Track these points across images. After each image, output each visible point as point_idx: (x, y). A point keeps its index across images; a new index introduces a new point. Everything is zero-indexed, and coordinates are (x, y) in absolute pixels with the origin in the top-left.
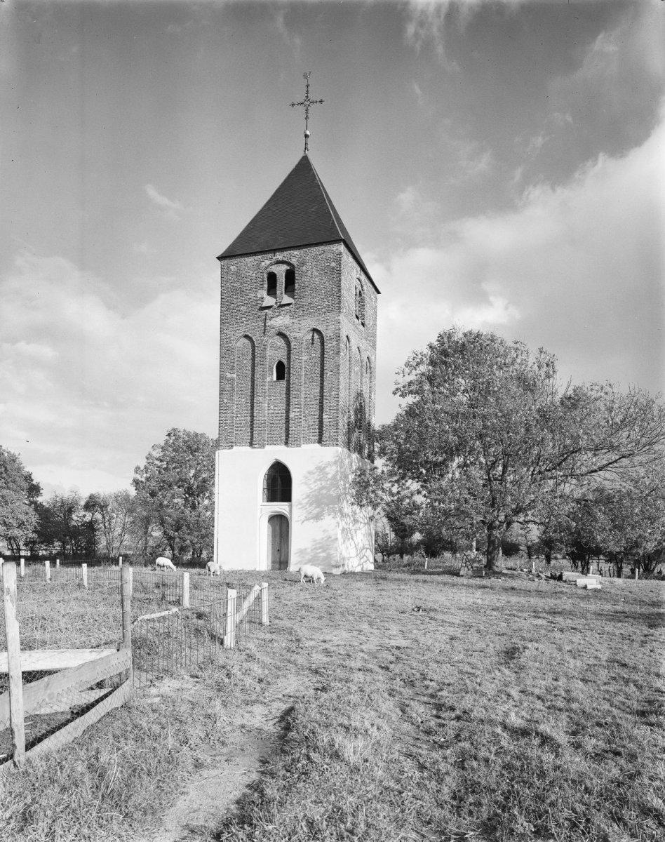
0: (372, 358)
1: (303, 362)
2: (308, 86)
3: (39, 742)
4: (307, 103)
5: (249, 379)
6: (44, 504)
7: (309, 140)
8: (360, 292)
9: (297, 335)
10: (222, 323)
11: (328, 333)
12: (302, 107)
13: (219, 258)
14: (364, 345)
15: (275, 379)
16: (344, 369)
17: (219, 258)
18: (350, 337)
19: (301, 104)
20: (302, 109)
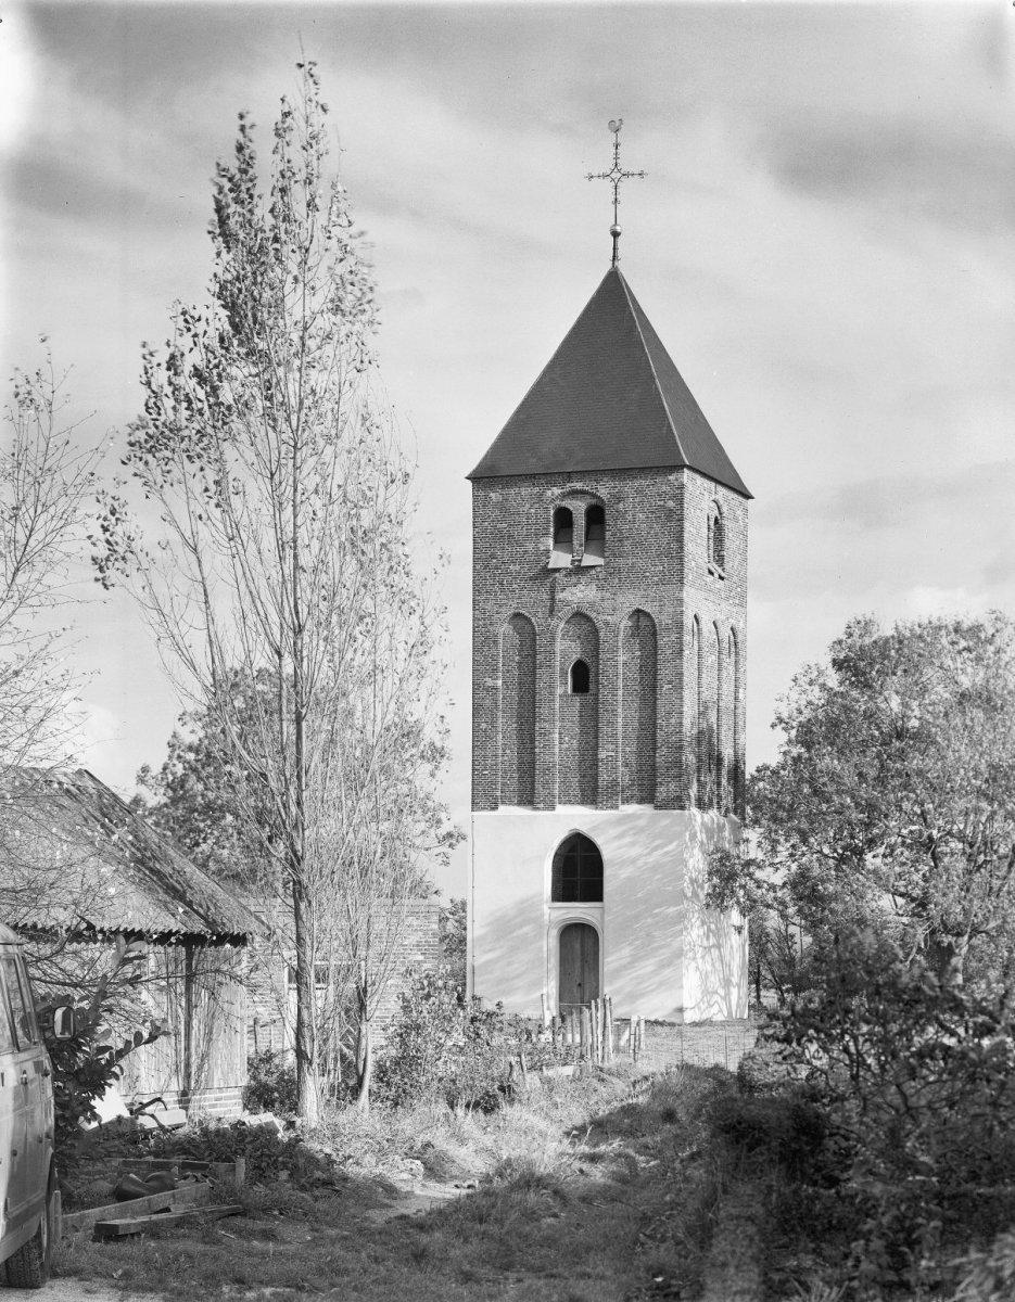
1: (620, 662)
18: (700, 616)
20: (608, 185)
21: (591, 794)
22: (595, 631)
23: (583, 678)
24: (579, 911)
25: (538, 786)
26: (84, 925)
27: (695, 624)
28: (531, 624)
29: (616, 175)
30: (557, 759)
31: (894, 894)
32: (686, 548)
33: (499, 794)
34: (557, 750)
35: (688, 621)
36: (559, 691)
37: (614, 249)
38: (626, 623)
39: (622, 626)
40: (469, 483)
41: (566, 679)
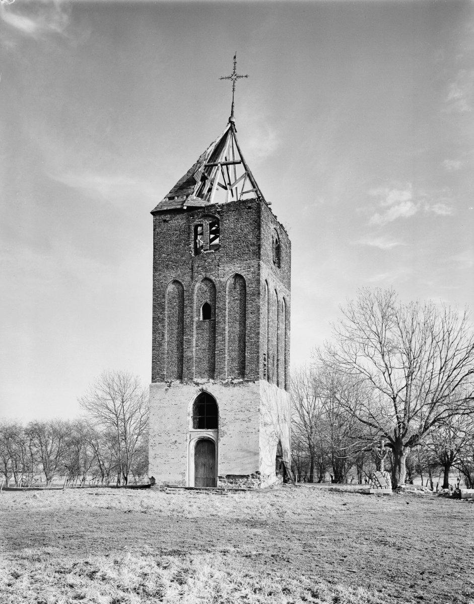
0: (287, 299)
1: (228, 304)
2: (235, 69)
3: (154, 340)
4: (234, 77)
5: (57, 491)
6: (28, 427)
7: (245, 78)
8: (276, 240)
9: (221, 279)
10: (155, 269)
11: (248, 276)
12: (229, 80)
13: (152, 213)
14: (281, 287)
15: (201, 319)
16: (264, 310)
17: (152, 213)
18: (269, 281)
19: (228, 78)
20: (230, 82)
21: (212, 372)
22: (214, 286)
23: (208, 311)
24: (208, 433)
25: (185, 369)
26: (255, 487)
27: (266, 286)
28: (182, 285)
29: (234, 77)
30: (194, 354)
31: (406, 385)
32: (261, 283)
33: (165, 373)
34: (194, 350)
35: (263, 282)
36: (196, 319)
37: (232, 106)
38: (232, 281)
39: (228, 283)
40: (152, 216)
41: (200, 312)
